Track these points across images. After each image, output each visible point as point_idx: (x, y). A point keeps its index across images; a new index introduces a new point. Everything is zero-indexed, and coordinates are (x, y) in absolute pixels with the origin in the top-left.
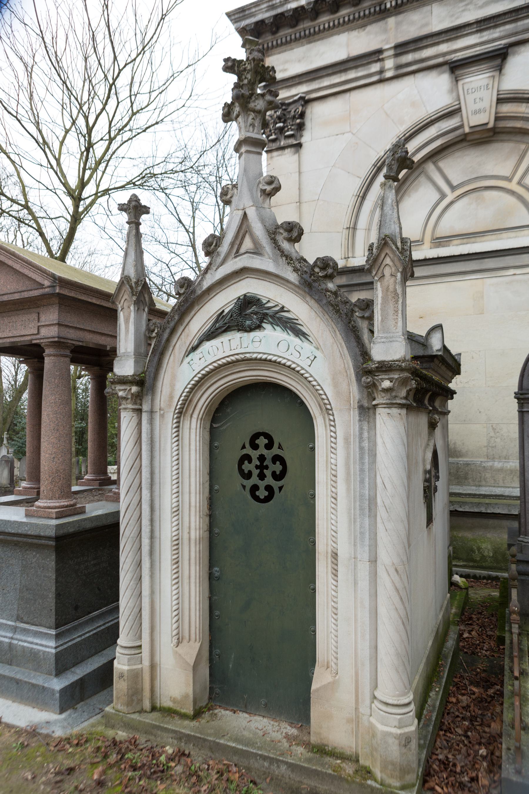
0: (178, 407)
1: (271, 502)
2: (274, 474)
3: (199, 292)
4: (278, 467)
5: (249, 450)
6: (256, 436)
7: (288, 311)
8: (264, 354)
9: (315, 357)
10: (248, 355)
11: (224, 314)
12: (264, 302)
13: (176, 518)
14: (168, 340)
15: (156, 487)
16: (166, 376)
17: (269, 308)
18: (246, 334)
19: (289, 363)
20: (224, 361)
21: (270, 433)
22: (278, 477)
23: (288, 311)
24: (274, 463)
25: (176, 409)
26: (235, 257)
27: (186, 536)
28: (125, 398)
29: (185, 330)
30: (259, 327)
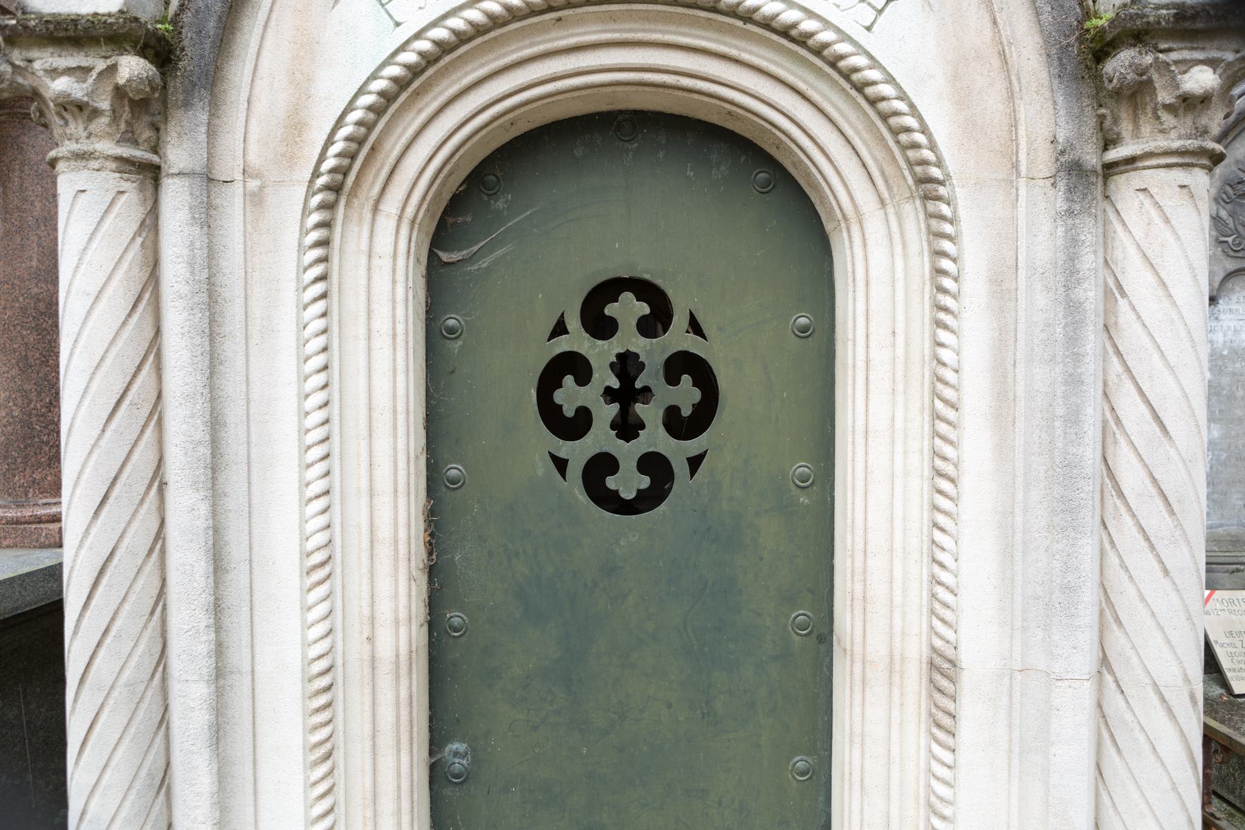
1: (663, 507)
5: (578, 340)
6: (609, 289)
13: (321, 591)
15: (234, 480)
16: (268, 43)
21: (659, 282)
24: (672, 380)
25: (316, 174)
27: (357, 649)
28: (80, 107)
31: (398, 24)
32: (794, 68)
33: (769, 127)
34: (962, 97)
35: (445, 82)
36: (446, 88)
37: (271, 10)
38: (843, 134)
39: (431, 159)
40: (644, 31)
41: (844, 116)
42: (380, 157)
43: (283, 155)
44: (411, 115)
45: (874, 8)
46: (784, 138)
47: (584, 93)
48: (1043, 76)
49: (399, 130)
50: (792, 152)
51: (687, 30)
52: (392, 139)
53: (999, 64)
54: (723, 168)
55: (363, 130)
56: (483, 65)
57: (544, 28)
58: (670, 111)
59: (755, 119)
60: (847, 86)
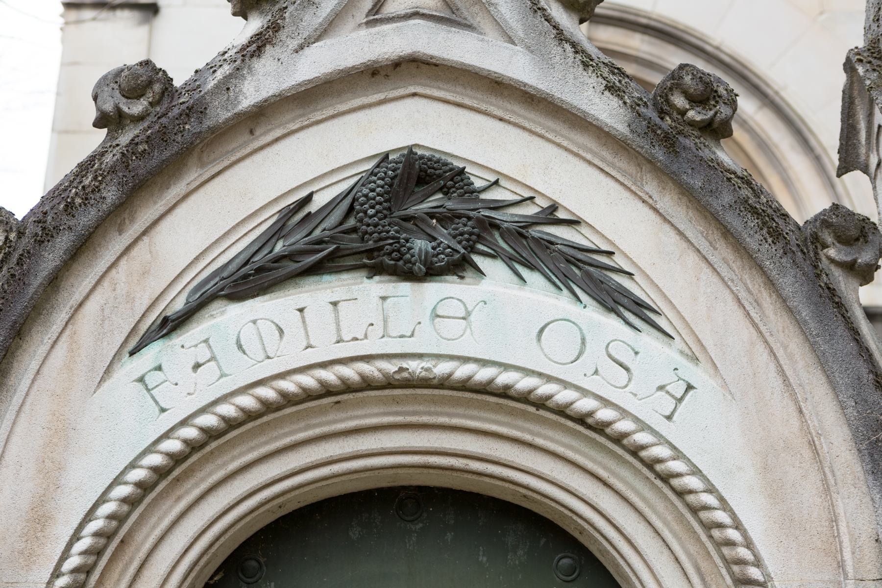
0: (74, 561)
3: (220, 114)
7: (573, 223)
8: (484, 363)
9: (690, 387)
10: (415, 367)
11: (313, 207)
12: (478, 184)
14: (55, 282)
16: (18, 429)
17: (499, 206)
18: (405, 287)
19: (584, 405)
20: (308, 381)
23: (573, 223)
26: (370, 24)
29: (135, 252)
30: (459, 266)
31: (163, 410)
32: (592, 453)
33: (570, 514)
34: (775, 491)
35: (209, 467)
36: (210, 474)
37: (27, 395)
38: (650, 524)
39: (186, 551)
40: (430, 414)
41: (650, 506)
42: (129, 550)
43: (21, 552)
44: (169, 503)
45: (673, 396)
46: (586, 526)
47: (363, 475)
48: (858, 468)
49: (153, 520)
50: (596, 540)
51: (475, 413)
52: (145, 530)
53: (811, 454)
54: (520, 552)
55: (114, 523)
56: (252, 449)
57: (322, 411)
58: (459, 488)
59: (553, 504)
60: (652, 476)
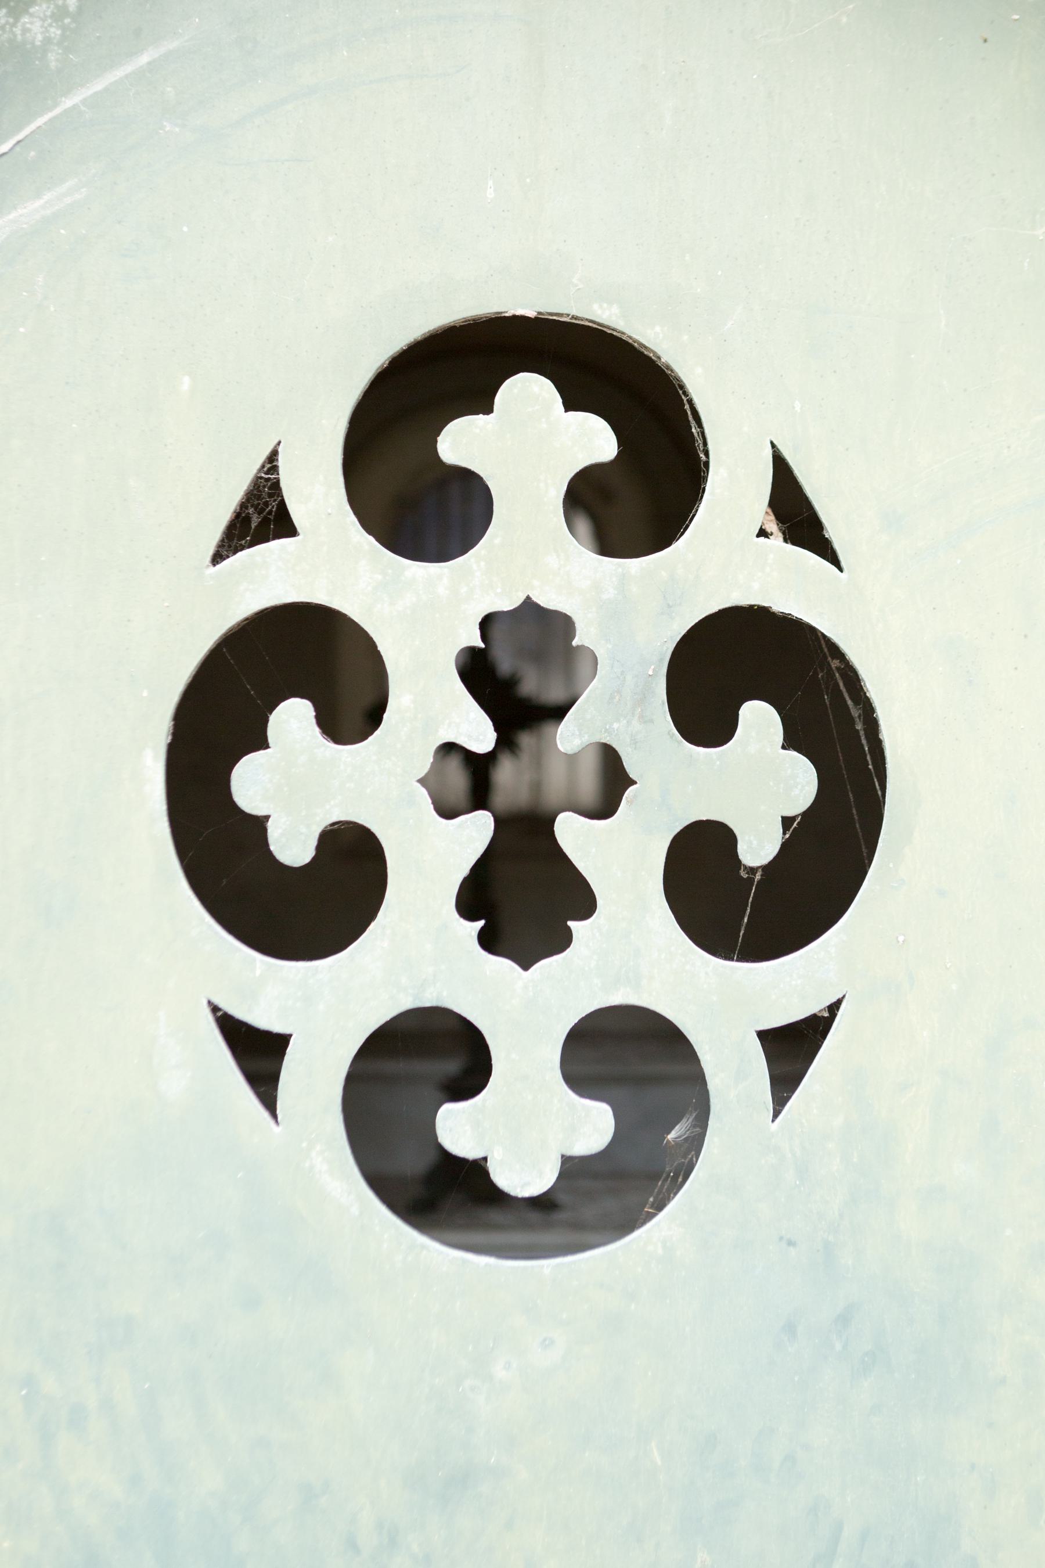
2: (353, 703)
4: (295, 782)
5: (332, 562)
6: (453, 366)
22: (303, 660)
